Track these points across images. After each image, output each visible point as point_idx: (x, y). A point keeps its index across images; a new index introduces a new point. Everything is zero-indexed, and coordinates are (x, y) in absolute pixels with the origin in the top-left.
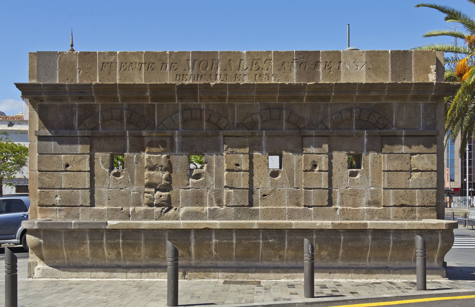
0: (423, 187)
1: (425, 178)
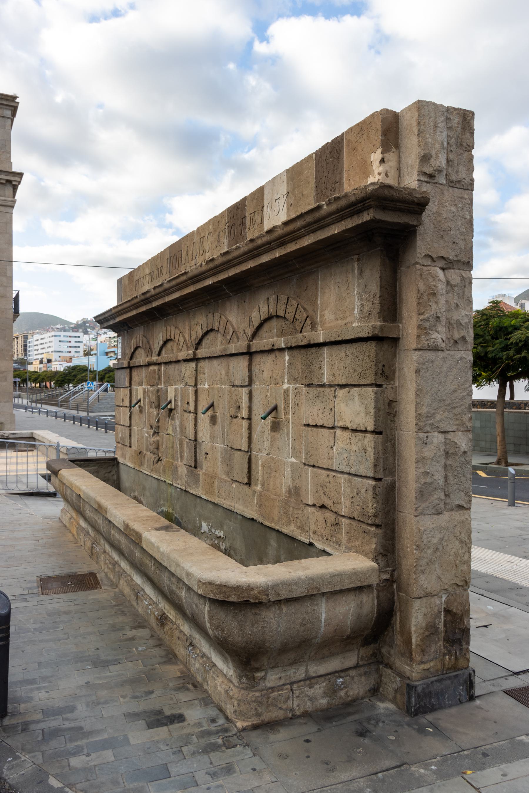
0: (353, 471)
1: (354, 448)
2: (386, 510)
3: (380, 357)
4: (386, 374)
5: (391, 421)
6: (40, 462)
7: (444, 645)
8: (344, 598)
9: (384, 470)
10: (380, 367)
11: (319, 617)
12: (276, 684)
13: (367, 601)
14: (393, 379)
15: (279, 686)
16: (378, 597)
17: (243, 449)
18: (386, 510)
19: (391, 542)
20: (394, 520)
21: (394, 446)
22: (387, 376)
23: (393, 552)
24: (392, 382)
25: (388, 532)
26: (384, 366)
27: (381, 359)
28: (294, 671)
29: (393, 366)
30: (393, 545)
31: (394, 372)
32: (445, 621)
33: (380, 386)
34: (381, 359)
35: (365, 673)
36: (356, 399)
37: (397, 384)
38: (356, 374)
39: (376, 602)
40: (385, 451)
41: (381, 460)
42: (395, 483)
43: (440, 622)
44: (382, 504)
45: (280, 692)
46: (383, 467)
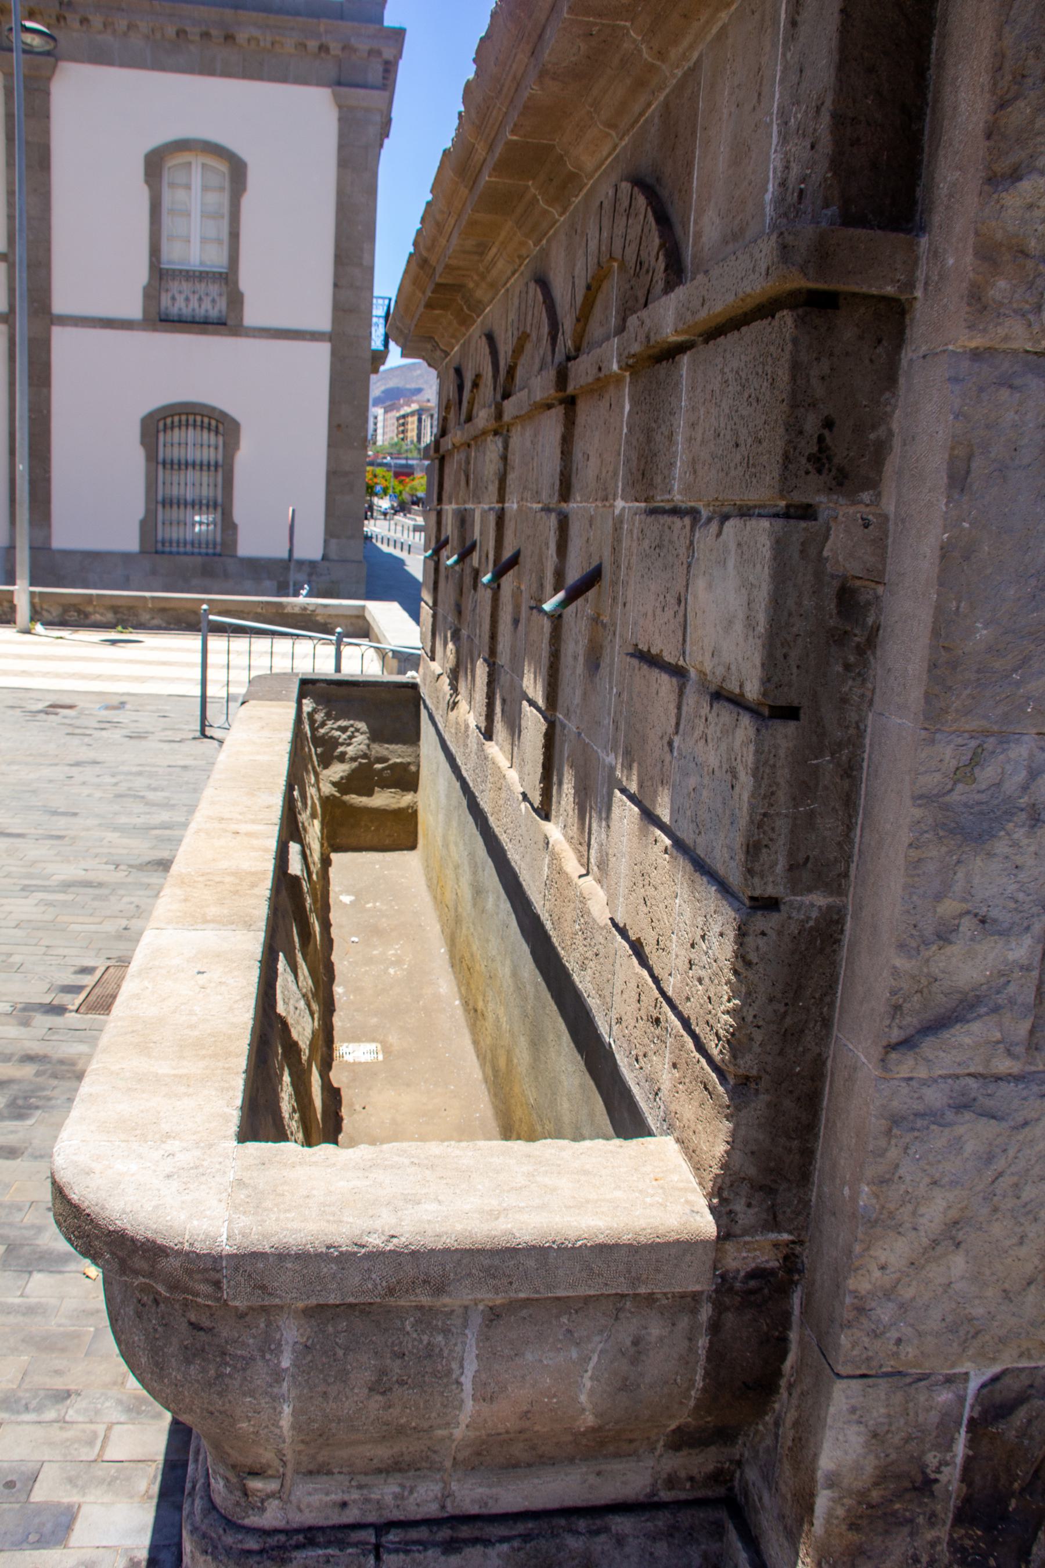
2: (788, 1021)
3: (814, 382)
4: (836, 461)
5: (847, 667)
6: (237, 667)
7: (952, 1542)
8: (564, 1319)
9: (791, 868)
10: (811, 423)
11: (449, 1372)
12: (327, 1518)
13: (661, 1339)
14: (873, 484)
15: (333, 1527)
16: (715, 1327)
17: (699, 660)
18: (788, 1021)
19: (796, 1143)
20: (819, 1062)
21: (850, 771)
22: (841, 470)
23: (805, 1177)
24: (866, 496)
25: (788, 1103)
26: (828, 424)
27: (819, 390)
28: (397, 1489)
29: (874, 427)
30: (808, 1154)
31: (880, 451)
32: (968, 1461)
33: (806, 512)
34: (819, 390)
35: (670, 1533)
36: (731, 563)
37: (889, 505)
38: (739, 457)
39: (703, 1342)
40: (805, 787)
41: (782, 826)
42: (840, 922)
43: (943, 1463)
44: (771, 1000)
45: (330, 1551)
46: (791, 854)
